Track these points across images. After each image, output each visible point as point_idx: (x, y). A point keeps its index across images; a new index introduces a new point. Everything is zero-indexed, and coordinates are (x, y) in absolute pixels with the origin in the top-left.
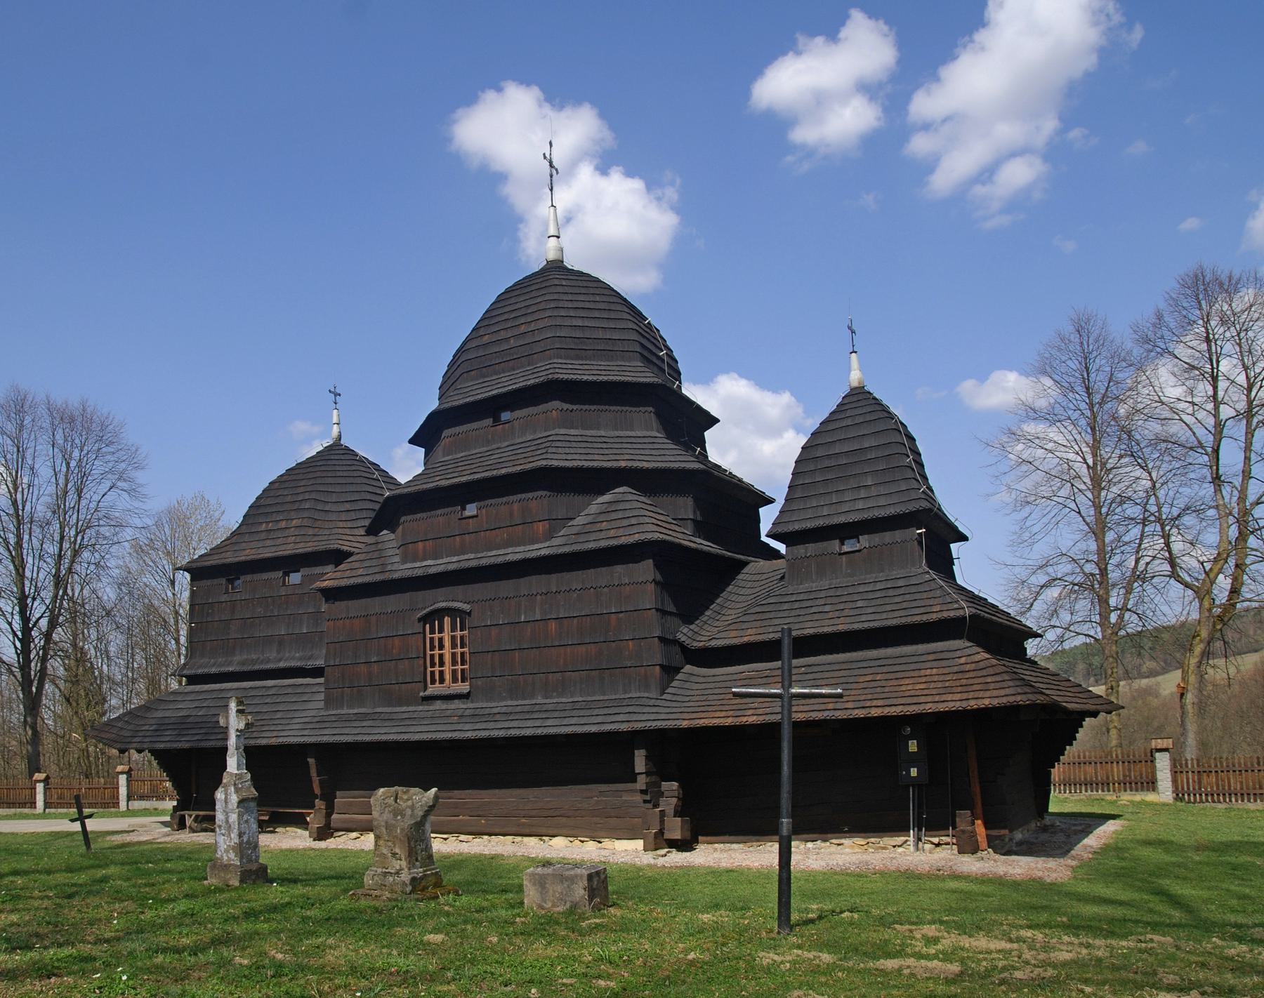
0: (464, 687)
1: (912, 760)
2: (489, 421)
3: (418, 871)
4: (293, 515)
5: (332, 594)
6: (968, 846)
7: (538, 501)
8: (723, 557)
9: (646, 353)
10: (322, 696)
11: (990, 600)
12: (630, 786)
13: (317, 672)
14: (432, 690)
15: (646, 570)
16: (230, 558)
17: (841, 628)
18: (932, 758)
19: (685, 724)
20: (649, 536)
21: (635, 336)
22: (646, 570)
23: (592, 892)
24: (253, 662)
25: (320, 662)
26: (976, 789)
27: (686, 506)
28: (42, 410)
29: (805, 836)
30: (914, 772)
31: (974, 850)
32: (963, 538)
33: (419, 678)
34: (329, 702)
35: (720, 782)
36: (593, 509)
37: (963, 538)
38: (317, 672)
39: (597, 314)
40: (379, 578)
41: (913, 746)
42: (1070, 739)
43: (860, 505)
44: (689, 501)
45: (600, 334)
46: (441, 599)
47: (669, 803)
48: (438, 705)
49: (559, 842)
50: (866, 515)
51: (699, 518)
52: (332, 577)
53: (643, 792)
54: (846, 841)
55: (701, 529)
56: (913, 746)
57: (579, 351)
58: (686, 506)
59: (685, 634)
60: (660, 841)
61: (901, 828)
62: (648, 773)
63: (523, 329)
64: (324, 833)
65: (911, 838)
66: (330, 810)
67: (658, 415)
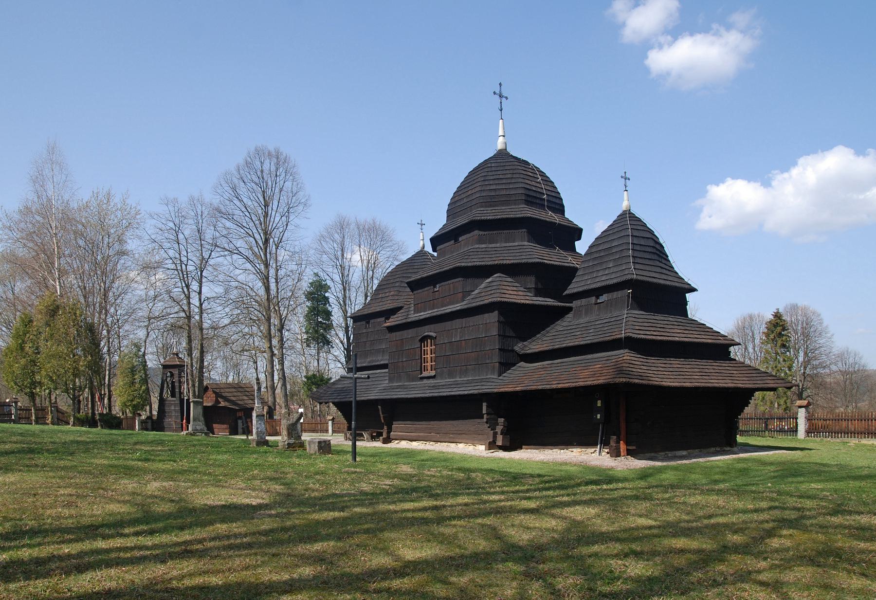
0: (433, 373)
1: (598, 410)
2: (453, 242)
3: (292, 441)
4: (392, 289)
5: (391, 329)
6: (616, 454)
7: (457, 283)
8: (558, 307)
9: (530, 199)
10: (387, 378)
11: (707, 325)
12: (479, 420)
13: (384, 366)
14: (425, 374)
15: (493, 317)
16: (366, 312)
17: (576, 343)
18: (607, 411)
19: (496, 390)
20: (495, 300)
21: (523, 191)
22: (493, 317)
23: (320, 448)
24: (374, 361)
25: (386, 362)
26: (623, 425)
27: (531, 281)
28: (353, 226)
29: (648, 455)
30: (599, 416)
31: (618, 455)
32: (693, 290)
33: (419, 368)
34: (391, 380)
35: (525, 419)
36: (483, 286)
37: (693, 290)
38: (384, 366)
39: (504, 181)
40: (404, 321)
41: (599, 404)
42: (747, 404)
43: (604, 278)
44: (533, 279)
45: (504, 192)
46: (427, 331)
47: (499, 429)
48: (425, 381)
49: (461, 446)
50: (603, 284)
51: (540, 286)
52: (393, 321)
53: (487, 422)
54: (574, 450)
55: (538, 292)
56: (599, 404)
57: (491, 202)
58: (531, 281)
59: (520, 347)
60: (492, 446)
61: (593, 444)
62: (487, 414)
63: (470, 193)
64: (387, 440)
65: (598, 449)
66: (390, 430)
67: (528, 232)
